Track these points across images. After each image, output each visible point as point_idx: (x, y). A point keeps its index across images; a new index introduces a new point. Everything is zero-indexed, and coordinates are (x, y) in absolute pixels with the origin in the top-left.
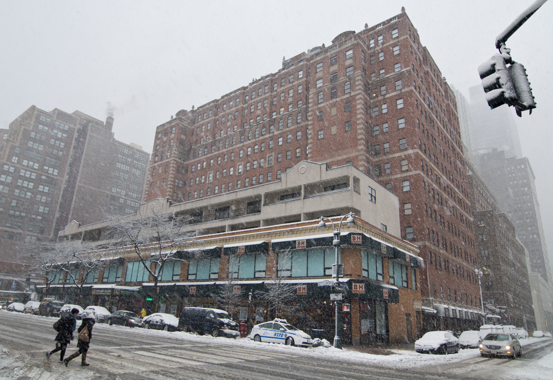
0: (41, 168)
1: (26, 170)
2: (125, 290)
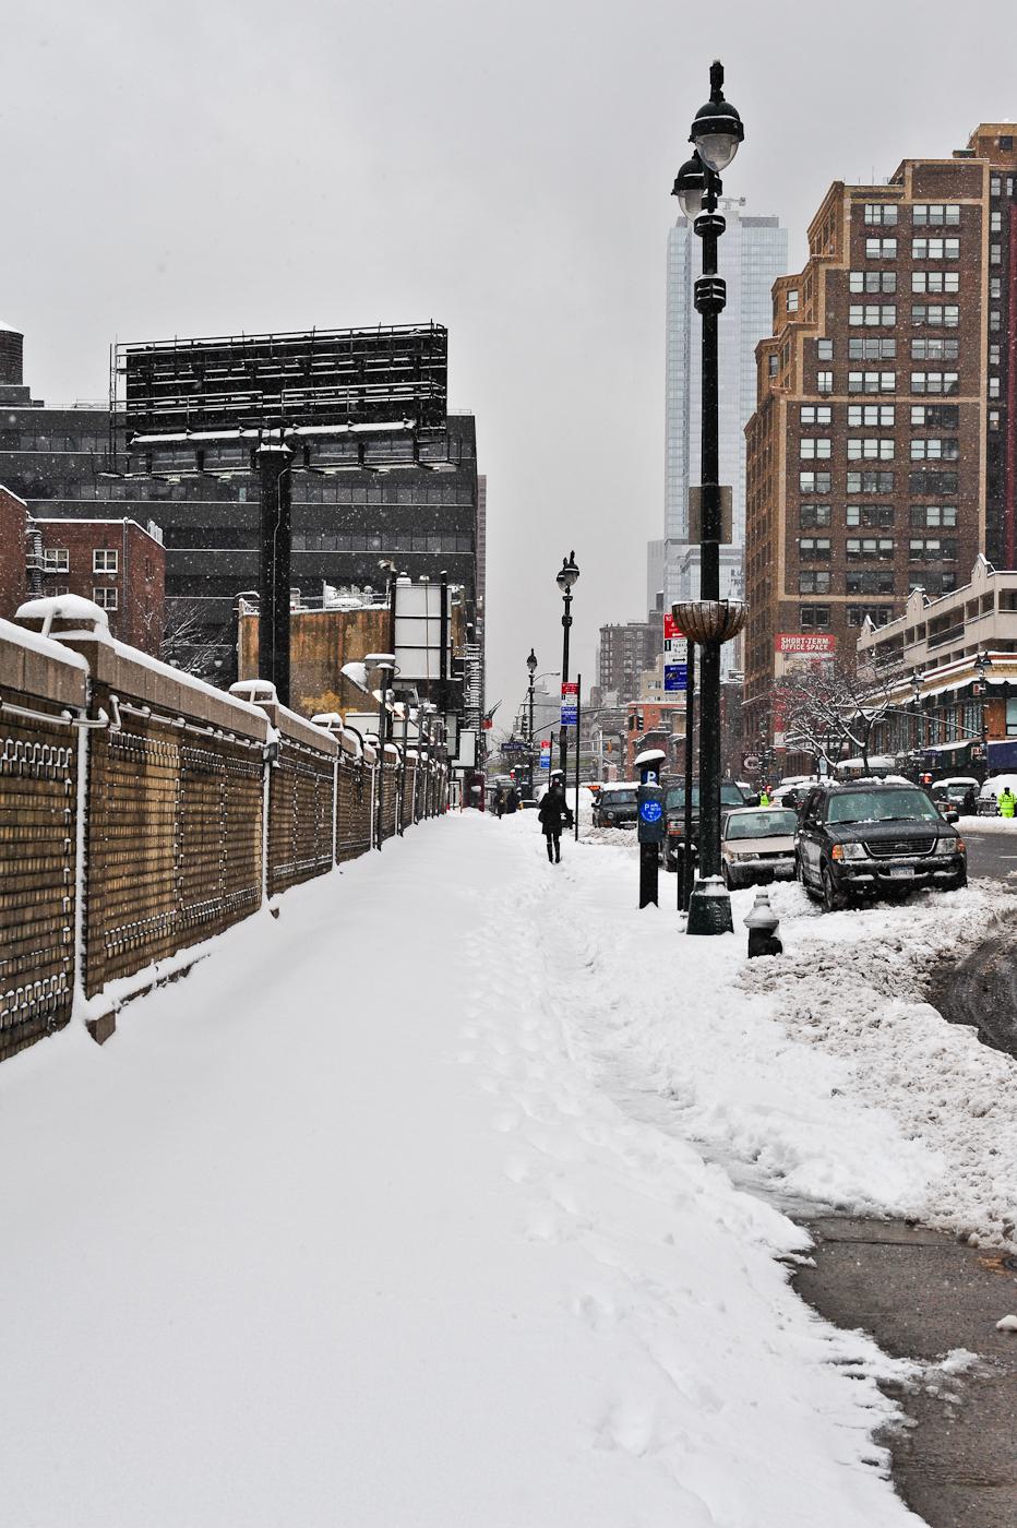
0: (903, 384)
1: (863, 406)
2: (156, 433)
